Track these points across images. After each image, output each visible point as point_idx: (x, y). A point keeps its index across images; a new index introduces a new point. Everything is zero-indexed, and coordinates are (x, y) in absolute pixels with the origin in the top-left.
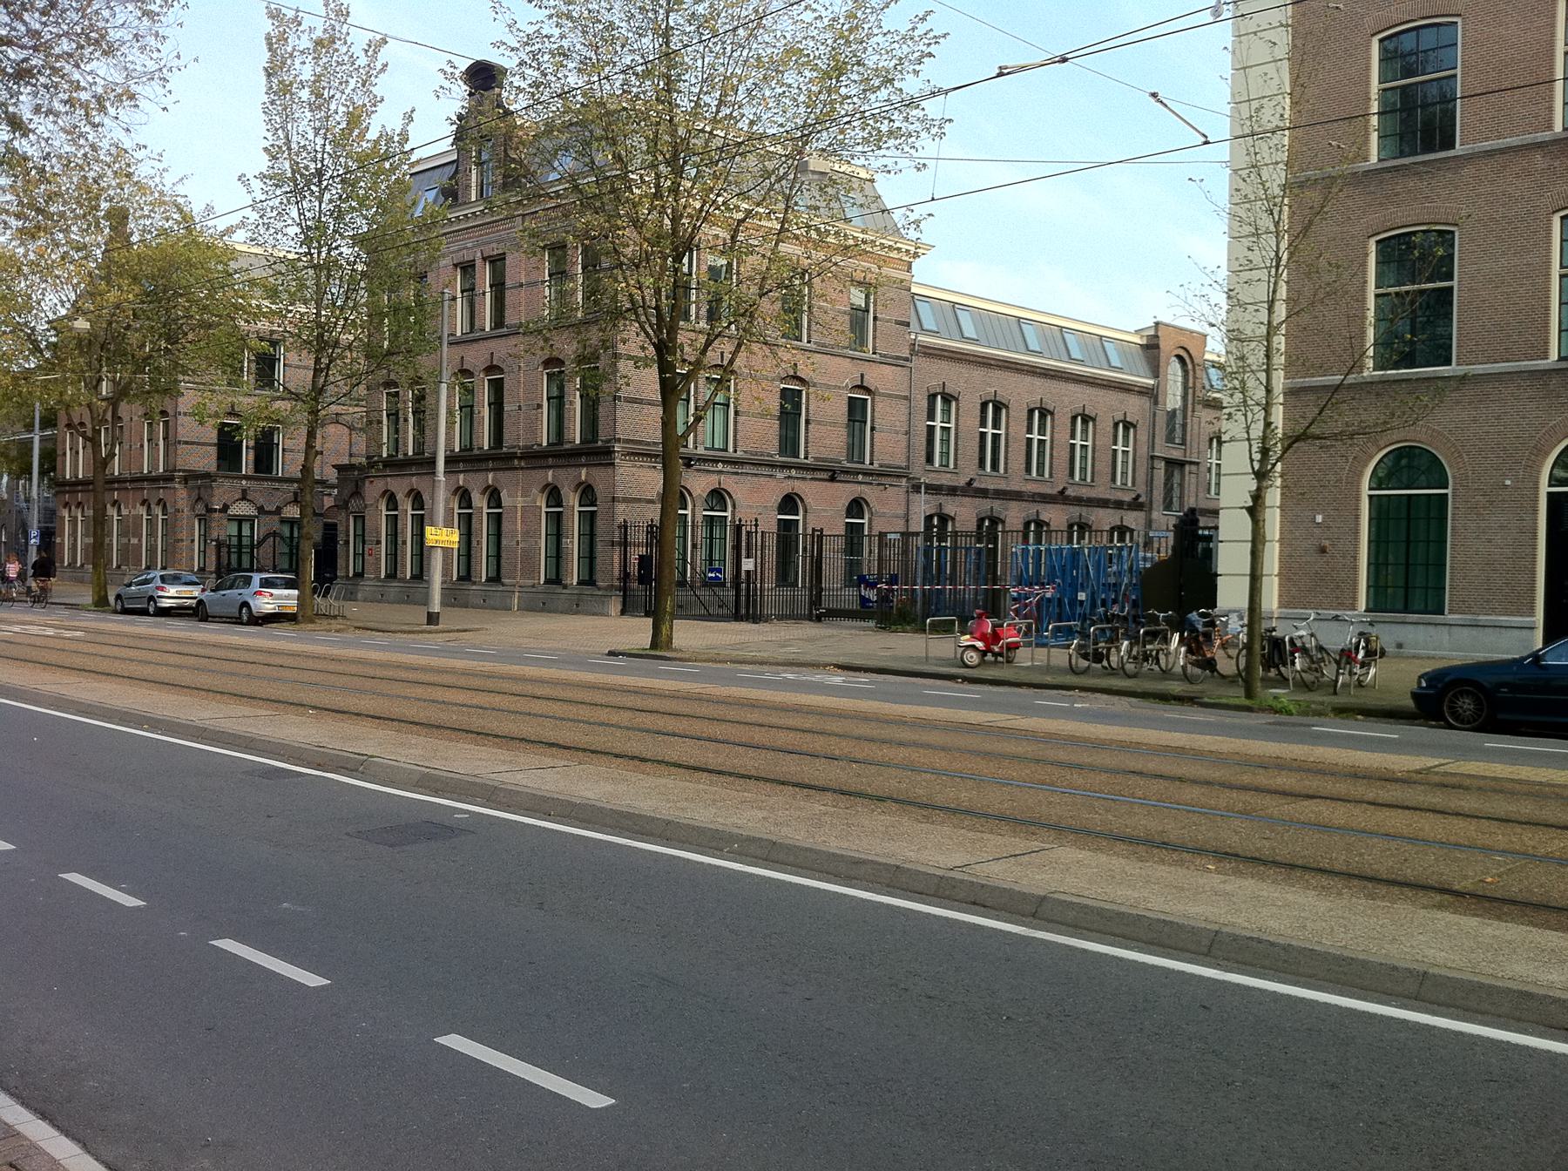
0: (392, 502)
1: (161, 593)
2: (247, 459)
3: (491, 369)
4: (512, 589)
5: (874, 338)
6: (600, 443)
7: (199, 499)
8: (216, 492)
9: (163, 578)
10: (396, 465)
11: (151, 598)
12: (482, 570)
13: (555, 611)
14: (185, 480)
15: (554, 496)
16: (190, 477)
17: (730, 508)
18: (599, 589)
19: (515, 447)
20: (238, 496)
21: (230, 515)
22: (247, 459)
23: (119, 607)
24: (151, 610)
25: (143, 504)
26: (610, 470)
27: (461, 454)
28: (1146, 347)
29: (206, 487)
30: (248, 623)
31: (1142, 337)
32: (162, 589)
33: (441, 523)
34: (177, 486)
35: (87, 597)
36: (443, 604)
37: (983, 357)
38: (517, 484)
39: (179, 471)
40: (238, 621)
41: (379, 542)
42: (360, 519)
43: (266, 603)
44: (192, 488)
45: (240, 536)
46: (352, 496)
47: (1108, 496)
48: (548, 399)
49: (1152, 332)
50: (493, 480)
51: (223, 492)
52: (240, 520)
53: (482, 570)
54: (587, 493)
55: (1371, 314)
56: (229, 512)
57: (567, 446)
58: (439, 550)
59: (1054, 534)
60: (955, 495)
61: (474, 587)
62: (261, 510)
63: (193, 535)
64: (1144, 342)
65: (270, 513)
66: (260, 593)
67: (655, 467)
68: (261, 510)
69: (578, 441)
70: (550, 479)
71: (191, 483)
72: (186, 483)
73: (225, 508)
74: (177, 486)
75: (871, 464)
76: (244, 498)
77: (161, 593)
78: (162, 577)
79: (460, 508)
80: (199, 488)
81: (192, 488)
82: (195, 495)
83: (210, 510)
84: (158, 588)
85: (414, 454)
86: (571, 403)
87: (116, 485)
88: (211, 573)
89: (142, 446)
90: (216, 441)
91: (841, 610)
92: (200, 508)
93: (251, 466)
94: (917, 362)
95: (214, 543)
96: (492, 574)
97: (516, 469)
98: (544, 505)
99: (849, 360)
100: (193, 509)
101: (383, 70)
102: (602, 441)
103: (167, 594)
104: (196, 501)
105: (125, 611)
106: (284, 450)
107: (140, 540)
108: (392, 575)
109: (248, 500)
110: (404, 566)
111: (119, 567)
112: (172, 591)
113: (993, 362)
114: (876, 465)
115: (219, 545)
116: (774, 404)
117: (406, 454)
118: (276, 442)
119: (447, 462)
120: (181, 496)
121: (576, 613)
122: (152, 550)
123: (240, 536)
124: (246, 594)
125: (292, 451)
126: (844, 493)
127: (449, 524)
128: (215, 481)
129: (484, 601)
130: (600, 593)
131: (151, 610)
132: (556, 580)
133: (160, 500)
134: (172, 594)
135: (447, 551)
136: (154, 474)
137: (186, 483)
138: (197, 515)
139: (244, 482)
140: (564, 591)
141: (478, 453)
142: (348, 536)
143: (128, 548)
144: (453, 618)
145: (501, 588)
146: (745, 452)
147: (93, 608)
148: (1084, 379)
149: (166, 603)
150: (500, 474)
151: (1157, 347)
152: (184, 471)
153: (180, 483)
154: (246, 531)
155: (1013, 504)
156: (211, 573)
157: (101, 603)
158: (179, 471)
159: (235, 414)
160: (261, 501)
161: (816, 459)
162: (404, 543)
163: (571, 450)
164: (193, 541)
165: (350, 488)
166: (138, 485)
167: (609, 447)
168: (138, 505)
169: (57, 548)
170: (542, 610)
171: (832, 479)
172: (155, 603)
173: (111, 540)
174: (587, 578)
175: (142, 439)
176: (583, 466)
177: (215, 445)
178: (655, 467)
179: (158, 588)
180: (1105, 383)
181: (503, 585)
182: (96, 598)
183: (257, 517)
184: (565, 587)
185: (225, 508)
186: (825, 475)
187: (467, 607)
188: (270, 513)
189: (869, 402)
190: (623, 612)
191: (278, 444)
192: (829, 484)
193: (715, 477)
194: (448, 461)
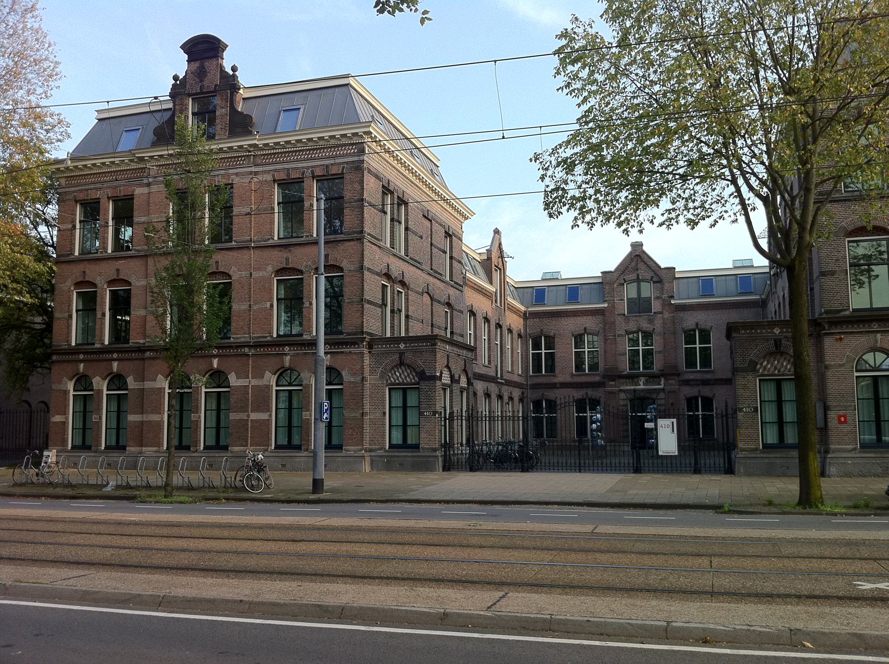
27: (279, 339)
63: (384, 407)
76: (401, 364)
107: (270, 415)
175: (70, 311)
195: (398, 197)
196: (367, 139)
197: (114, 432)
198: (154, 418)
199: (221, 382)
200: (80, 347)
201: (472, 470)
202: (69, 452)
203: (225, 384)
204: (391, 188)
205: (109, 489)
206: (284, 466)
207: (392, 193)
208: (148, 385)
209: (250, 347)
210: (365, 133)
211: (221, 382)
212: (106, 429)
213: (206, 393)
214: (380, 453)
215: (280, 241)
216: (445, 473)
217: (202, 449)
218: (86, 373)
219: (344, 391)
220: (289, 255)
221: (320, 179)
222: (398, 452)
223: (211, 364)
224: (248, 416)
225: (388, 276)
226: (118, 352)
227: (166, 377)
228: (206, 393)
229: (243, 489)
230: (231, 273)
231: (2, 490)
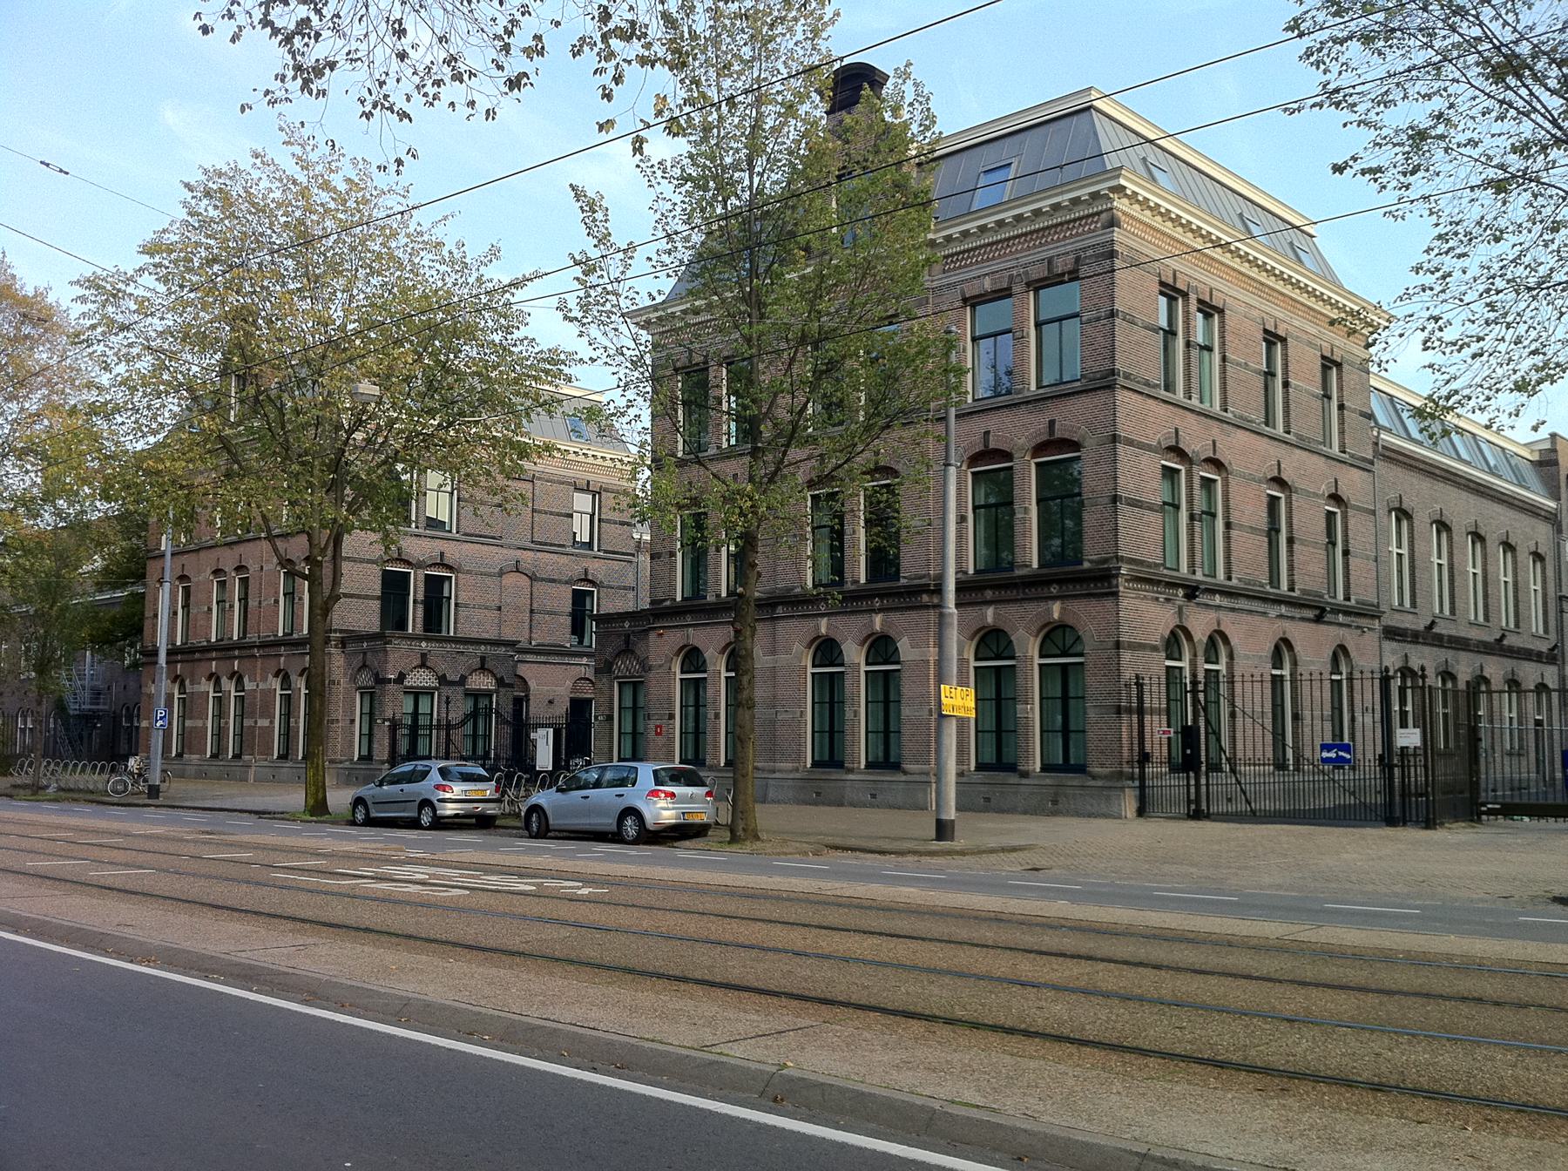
0: (693, 658)
1: (443, 795)
2: (415, 617)
3: (1050, 444)
4: (924, 778)
5: (1342, 432)
6: (1086, 565)
7: (364, 666)
8: (391, 657)
9: (444, 772)
10: (697, 608)
11: (426, 803)
12: (860, 749)
13: (1012, 810)
14: (343, 643)
15: (827, 650)
16: (350, 639)
17: (1224, 659)
18: (1094, 777)
19: (923, 577)
20: (417, 662)
21: (406, 687)
22: (415, 617)
23: (360, 816)
24: (426, 819)
25: (209, 678)
26: (1108, 603)
27: (685, 603)
28: (1538, 464)
29: (375, 651)
30: (431, 828)
31: (1532, 451)
32: (443, 788)
33: (955, 682)
34: (333, 650)
35: (296, 798)
36: (958, 809)
37: (1431, 465)
38: (928, 630)
39: (335, 631)
40: (616, 837)
41: (672, 717)
42: (636, 686)
43: (662, 812)
44: (355, 653)
45: (415, 714)
46: (618, 655)
47: (1531, 647)
48: (975, 508)
49: (1547, 446)
50: (828, 628)
51: (398, 657)
52: (417, 694)
53: (860, 749)
54: (1057, 638)
55: (863, 547)
56: (406, 683)
57: (1018, 572)
58: (954, 722)
59: (1495, 696)
60: (1418, 643)
61: (851, 777)
62: (442, 680)
63: (353, 712)
64: (1536, 457)
65: (452, 683)
66: (654, 793)
67: (1157, 599)
68: (442, 680)
69: (1035, 565)
70: (990, 620)
71: (350, 648)
72: (344, 646)
73: (401, 678)
74: (333, 650)
75: (1347, 598)
76: (423, 665)
77: (443, 795)
78: (441, 770)
79: (814, 666)
80: (365, 654)
81: (355, 653)
82: (359, 659)
83: (381, 681)
84: (438, 787)
85: (1041, 566)
86: (1026, 510)
87: (236, 653)
88: (383, 762)
89: (277, 602)
90: (379, 593)
91: (1525, 806)
92: (365, 679)
93: (420, 625)
94: (1380, 467)
95: (387, 723)
96: (365, 752)
97: (927, 607)
98: (972, 658)
99: (1323, 459)
100: (353, 679)
101: (832, 21)
102: (1090, 561)
103: (448, 796)
104: (359, 670)
105: (370, 822)
106: (456, 605)
107: (272, 722)
108: (283, 757)
109: (428, 668)
110: (716, 747)
111: (237, 756)
112: (458, 789)
113: (1437, 471)
114: (1353, 602)
115: (394, 726)
116: (567, 605)
117: (718, 596)
118: (446, 594)
119: (958, 590)
120: (337, 664)
121: (1054, 813)
122: (220, 734)
123: (415, 714)
124: (424, 788)
125: (466, 606)
126: (1328, 636)
127: (962, 683)
128: (390, 642)
129: (873, 796)
130: (1100, 783)
131: (426, 819)
132: (831, 758)
133: (234, 673)
134: (455, 796)
135: (962, 722)
136: (295, 636)
137: (344, 646)
138: (359, 688)
139: (424, 644)
140: (1024, 781)
141: (853, 587)
142: (612, 709)
143: (254, 732)
144: (978, 830)
145: (903, 778)
146: (1240, 580)
147: (308, 818)
148: (1505, 498)
149: (449, 810)
150: (895, 617)
151: (1555, 463)
152: (341, 631)
153: (336, 646)
154: (424, 707)
155: (1463, 655)
156: (383, 762)
157: (318, 808)
158: (335, 631)
159: (402, 560)
160: (442, 668)
161: (1303, 591)
162: (717, 716)
163: (1029, 576)
164: (353, 721)
165: (619, 643)
166: (272, 651)
167: (1109, 569)
168: (270, 676)
169: (142, 735)
170: (986, 810)
171: (1319, 619)
172: (434, 810)
173: (227, 723)
174: (881, 760)
175: (277, 593)
176: (1055, 598)
177: (378, 598)
178: (1157, 599)
179: (438, 787)
180: (1526, 506)
181: (905, 773)
182: (311, 802)
183: (436, 688)
184: (1025, 775)
185: (401, 678)
186: (1310, 614)
187: (841, 804)
188: (452, 683)
189: (1339, 517)
190: (1141, 812)
191: (450, 598)
192: (1313, 625)
193: (1212, 615)
194: (961, 588)
195: (1200, 301)
196: (1121, 204)
197: (691, 737)
198: (199, 723)
199: (1060, 645)
200: (689, 603)
201: (1391, 821)
202: (720, 771)
203: (1078, 649)
204: (1180, 285)
205: (50, 790)
206: (987, 800)
207: (1185, 295)
208: (783, 658)
209: (259, 647)
210: (1112, 189)
211: (1060, 645)
212: (977, 732)
213: (1041, 665)
214: (347, 764)
215: (976, 404)
216: (1141, 820)
217: (863, 766)
218: (1001, 625)
219: (1087, 668)
220: (287, 545)
221: (729, 362)
222: (823, 773)
223: (818, 628)
224: (256, 722)
225: (1177, 451)
226: (881, 596)
227: (862, 644)
228: (1041, 665)
229: (106, 793)
230: (898, 467)
231: (2, 792)
